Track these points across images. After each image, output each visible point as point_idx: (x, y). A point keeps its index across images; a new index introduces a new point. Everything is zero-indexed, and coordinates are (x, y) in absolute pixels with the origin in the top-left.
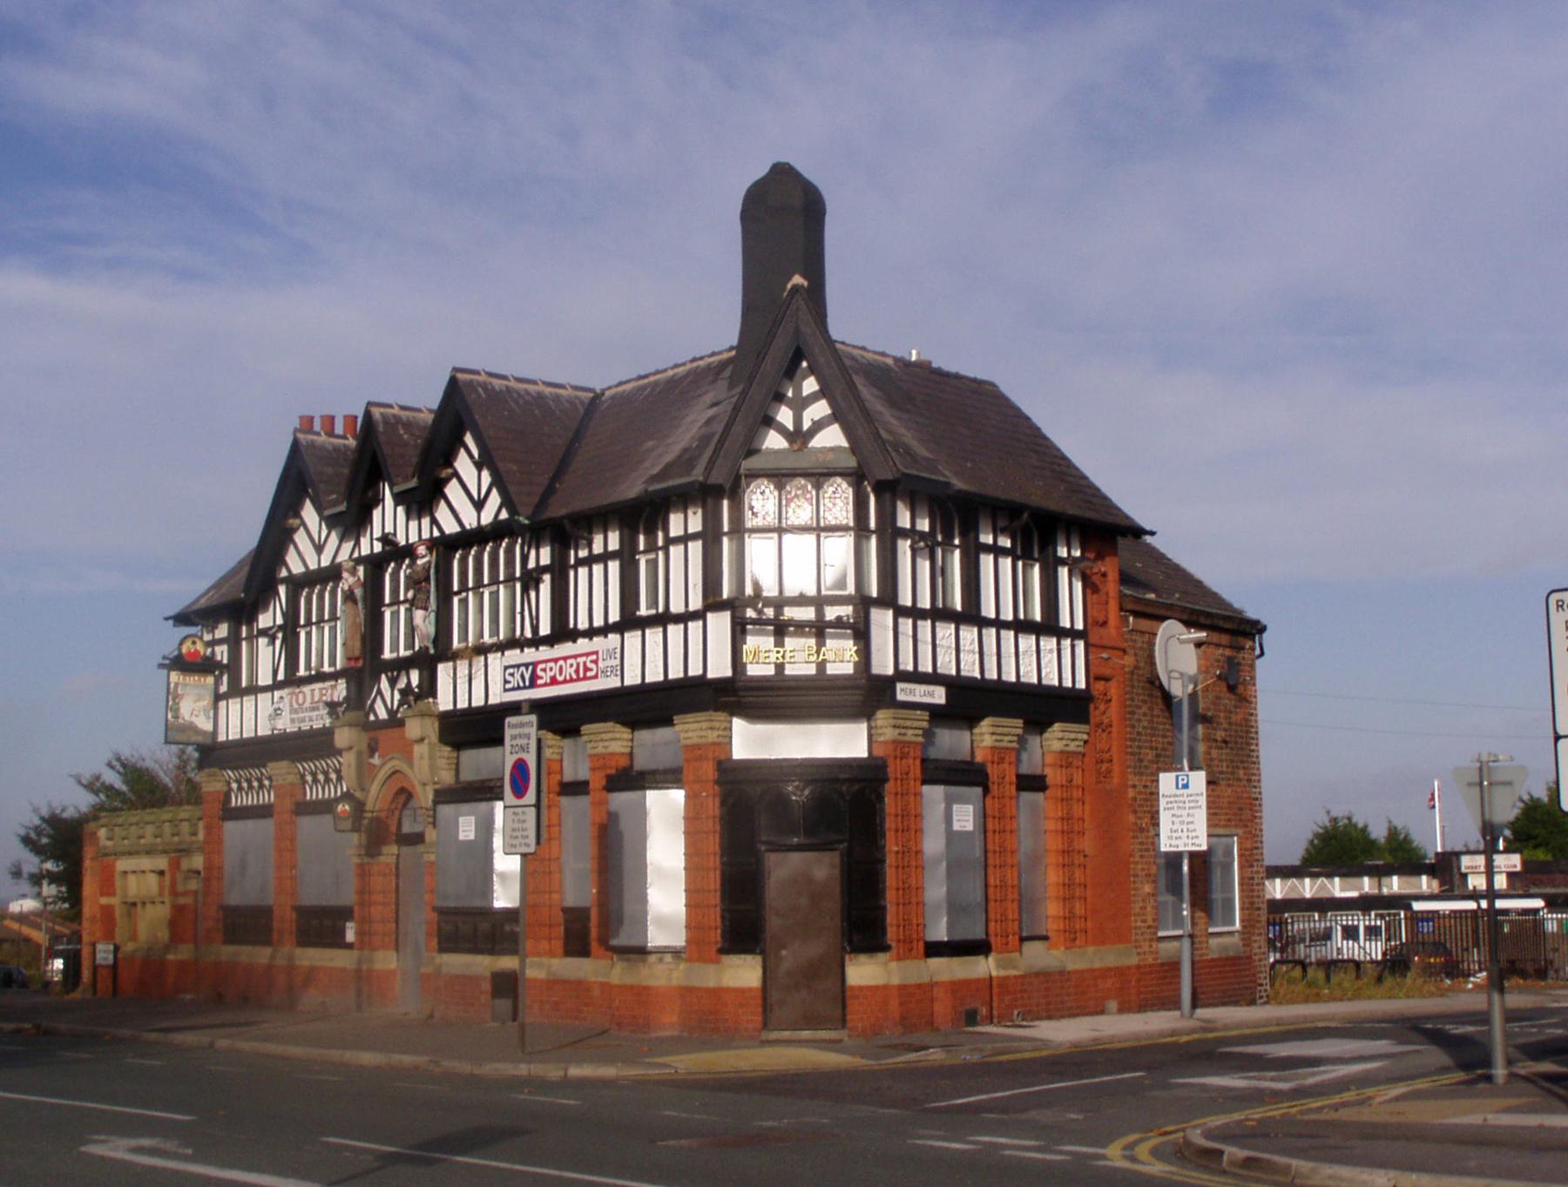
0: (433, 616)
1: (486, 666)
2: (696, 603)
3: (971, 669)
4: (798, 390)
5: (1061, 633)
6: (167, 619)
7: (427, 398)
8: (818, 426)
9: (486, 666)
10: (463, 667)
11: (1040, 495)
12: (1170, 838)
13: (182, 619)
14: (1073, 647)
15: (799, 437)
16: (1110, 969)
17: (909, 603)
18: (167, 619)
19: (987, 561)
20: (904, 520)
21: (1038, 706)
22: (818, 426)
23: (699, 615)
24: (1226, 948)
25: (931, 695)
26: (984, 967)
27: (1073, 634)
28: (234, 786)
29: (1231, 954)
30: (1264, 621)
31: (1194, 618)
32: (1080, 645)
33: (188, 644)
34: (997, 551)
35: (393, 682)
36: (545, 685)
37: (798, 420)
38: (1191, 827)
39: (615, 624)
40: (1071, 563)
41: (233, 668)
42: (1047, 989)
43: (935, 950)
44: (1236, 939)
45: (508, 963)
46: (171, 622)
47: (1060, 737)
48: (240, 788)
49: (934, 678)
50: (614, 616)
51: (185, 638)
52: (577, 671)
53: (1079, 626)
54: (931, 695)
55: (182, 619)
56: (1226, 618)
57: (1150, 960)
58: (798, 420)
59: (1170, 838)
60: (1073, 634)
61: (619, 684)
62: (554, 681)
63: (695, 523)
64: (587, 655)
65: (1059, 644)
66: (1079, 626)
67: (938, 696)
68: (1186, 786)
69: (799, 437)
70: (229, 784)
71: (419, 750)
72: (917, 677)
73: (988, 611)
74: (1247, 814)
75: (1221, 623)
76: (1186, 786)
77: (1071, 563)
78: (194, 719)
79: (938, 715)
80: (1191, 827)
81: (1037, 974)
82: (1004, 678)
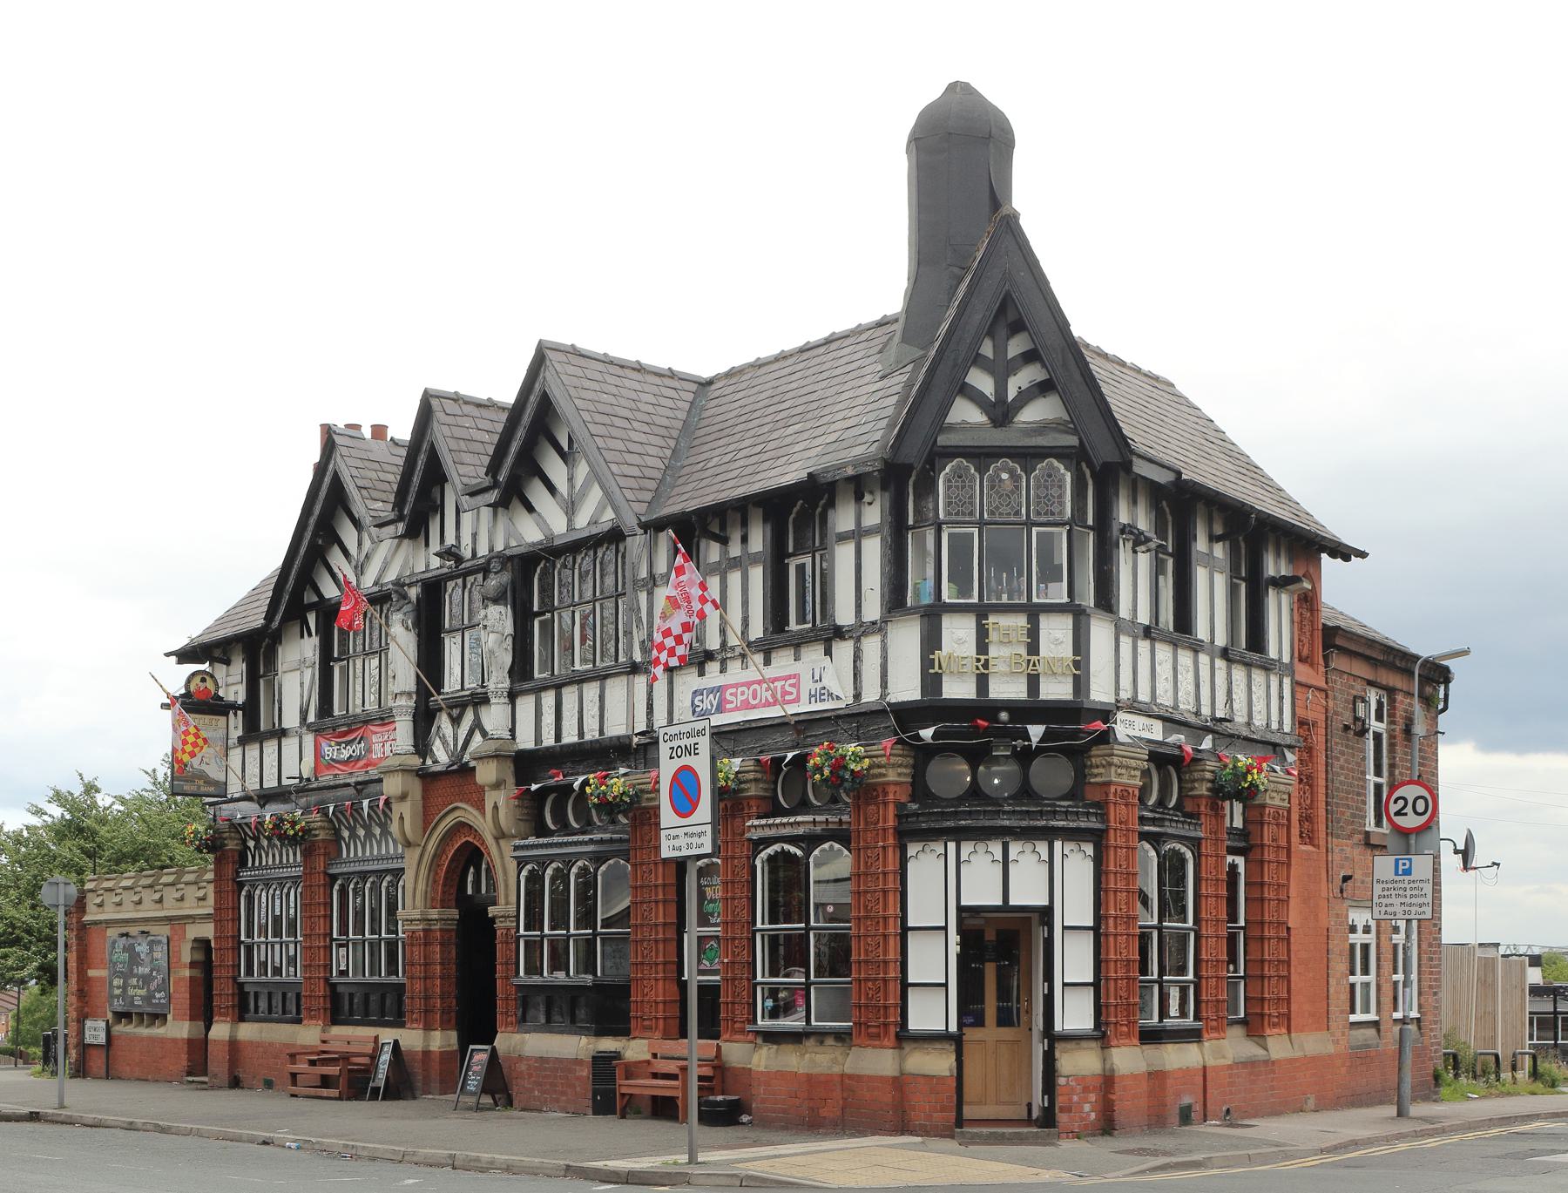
1: (602, 698)
2: (872, 611)
4: (1000, 350)
6: (168, 655)
7: (502, 384)
8: (1025, 397)
9: (602, 698)
10: (548, 699)
13: (184, 656)
15: (1001, 413)
18: (168, 655)
22: (1025, 397)
23: (878, 628)
25: (1150, 730)
28: (251, 844)
33: (197, 679)
35: (456, 721)
36: (737, 709)
37: (1001, 388)
39: (759, 640)
41: (250, 710)
45: (608, 1044)
46: (174, 658)
48: (258, 846)
50: (757, 631)
51: (194, 674)
52: (773, 696)
54: (1150, 730)
55: (184, 656)
58: (1001, 388)
62: (747, 706)
63: (873, 515)
64: (786, 678)
65: (1249, 677)
69: (1001, 413)
70: (244, 842)
71: (490, 798)
72: (1134, 707)
76: (1408, 872)
78: (204, 767)
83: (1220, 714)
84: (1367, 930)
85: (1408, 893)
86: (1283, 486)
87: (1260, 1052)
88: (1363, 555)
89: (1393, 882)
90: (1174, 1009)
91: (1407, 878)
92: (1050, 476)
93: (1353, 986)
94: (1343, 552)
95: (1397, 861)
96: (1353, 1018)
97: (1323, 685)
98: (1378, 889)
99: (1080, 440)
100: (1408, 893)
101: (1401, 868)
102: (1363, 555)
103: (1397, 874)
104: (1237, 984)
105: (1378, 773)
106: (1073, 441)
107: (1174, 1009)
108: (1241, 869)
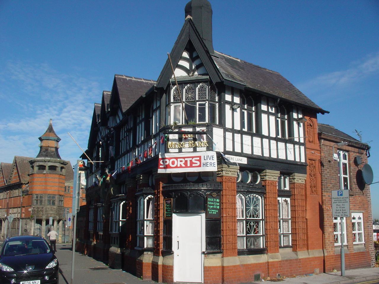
0: (114, 147)
3: (257, 152)
5: (295, 143)
11: (283, 95)
12: (336, 213)
14: (300, 148)
16: (316, 258)
17: (301, 147)
19: (264, 117)
20: (295, 115)
21: (287, 168)
24: (359, 249)
26: (263, 258)
27: (299, 144)
29: (362, 251)
30: (369, 145)
31: (350, 144)
32: (302, 148)
34: (268, 113)
38: (344, 209)
40: (298, 121)
42: (290, 266)
43: (241, 253)
44: (363, 246)
47: (300, 178)
49: (241, 154)
53: (302, 141)
54: (241, 160)
56: (356, 143)
57: (332, 254)
59: (336, 213)
60: (299, 144)
61: (282, 198)
65: (294, 147)
66: (302, 141)
67: (244, 161)
68: (341, 195)
72: (234, 153)
73: (265, 132)
74: (366, 206)
75: (355, 145)
76: (341, 195)
77: (298, 121)
79: (243, 168)
80: (344, 209)
81: (287, 261)
82: (272, 156)
83: (229, 148)
84: (360, 218)
85: (342, 201)
86: (307, 96)
87: (295, 256)
88: (328, 112)
89: (337, 198)
90: (101, 220)
91: (341, 197)
92: (202, 88)
93: (355, 234)
94: (323, 112)
95: (338, 192)
96: (354, 243)
97: (319, 149)
98: (333, 200)
99: (210, 77)
100: (342, 201)
101: (339, 194)
102: (328, 112)
103: (338, 195)
104: (281, 236)
105: (345, 173)
106: (208, 77)
107: (101, 220)
108: (289, 202)
